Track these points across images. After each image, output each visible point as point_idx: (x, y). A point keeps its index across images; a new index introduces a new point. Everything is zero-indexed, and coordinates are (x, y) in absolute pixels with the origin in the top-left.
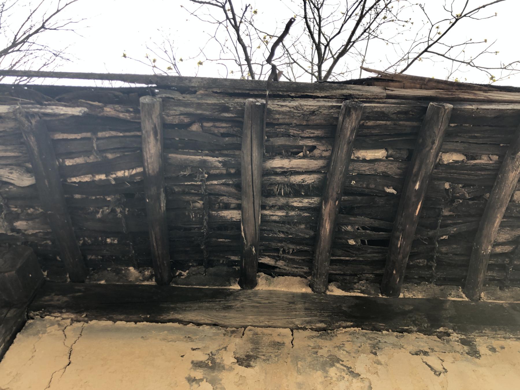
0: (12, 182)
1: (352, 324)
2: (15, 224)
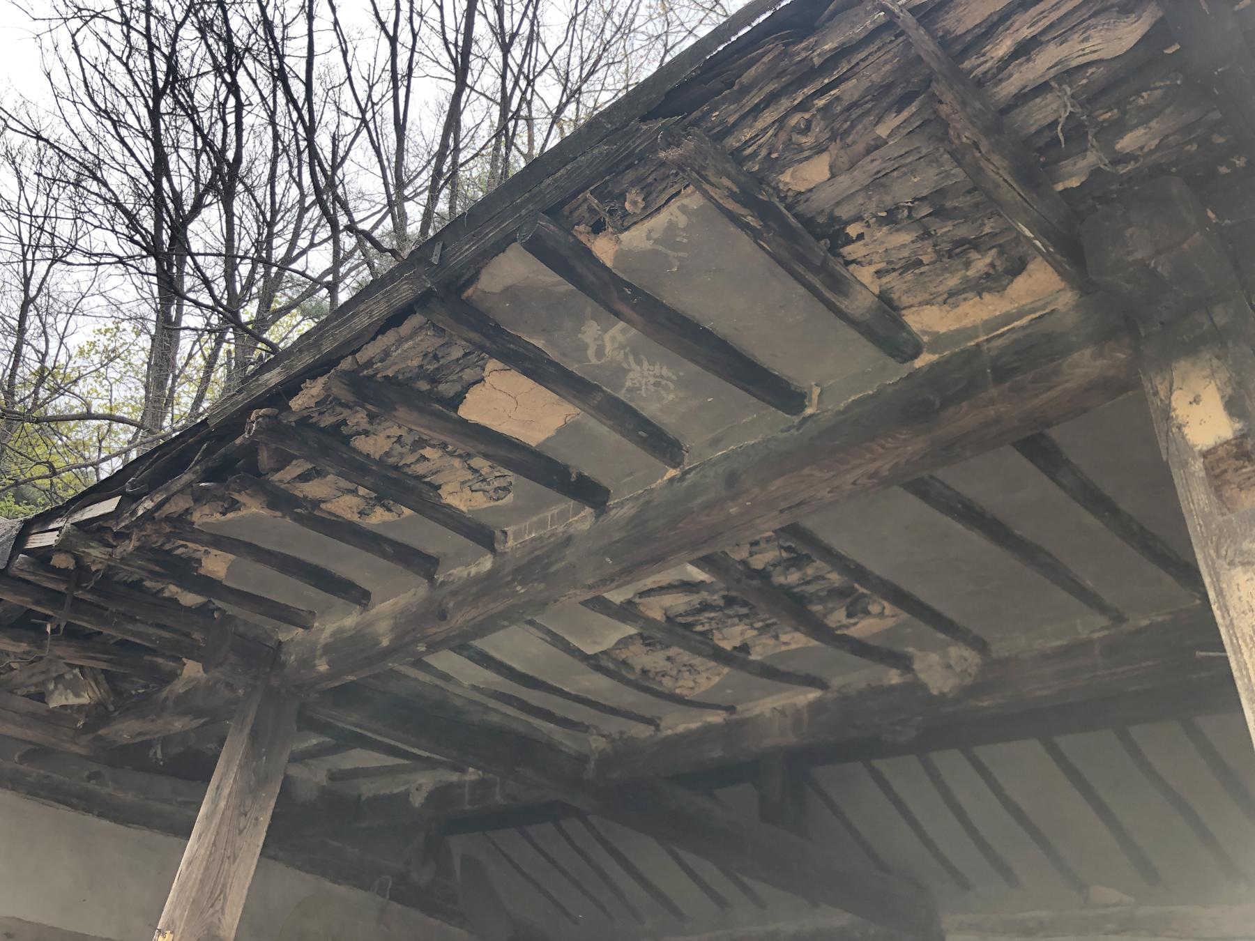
0: (1095, 57)
1: (452, 135)
2: (1118, 147)
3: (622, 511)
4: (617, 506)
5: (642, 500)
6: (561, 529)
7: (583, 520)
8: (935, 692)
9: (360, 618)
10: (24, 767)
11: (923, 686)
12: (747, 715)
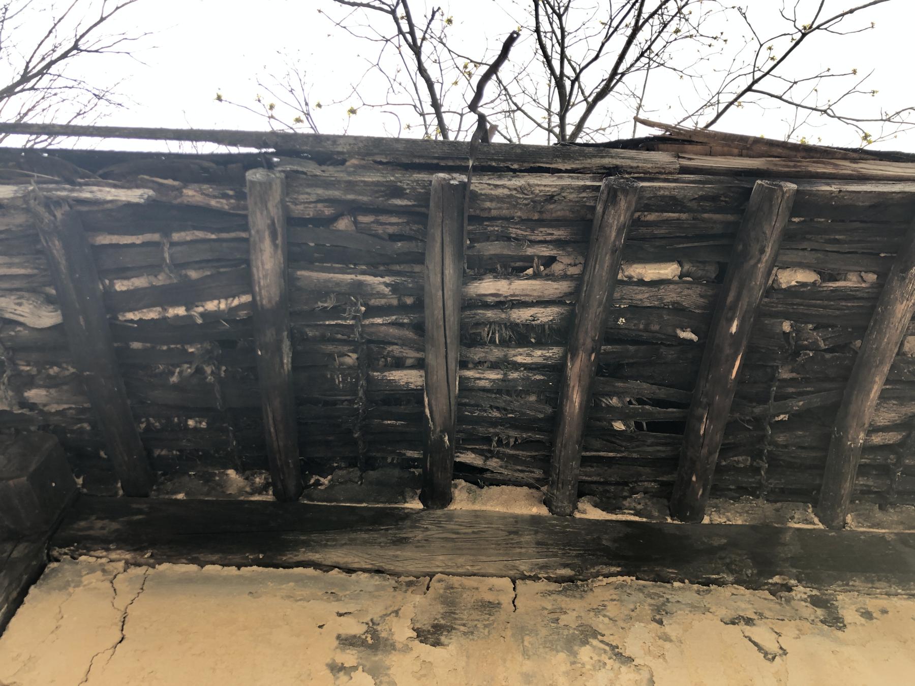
0: (21, 319)
1: (619, 569)
2: (26, 394)
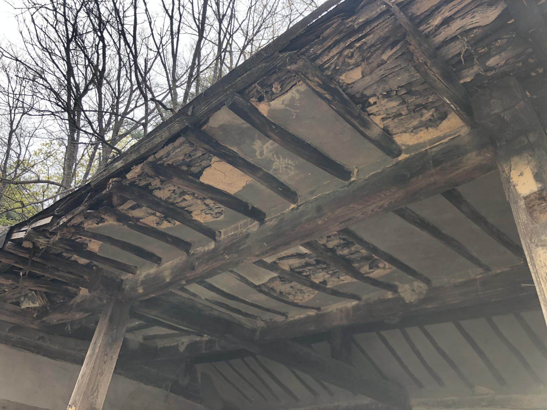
0: (477, 25)
1: (197, 59)
2: (487, 64)
3: (271, 223)
4: (269, 220)
5: (280, 218)
6: (244, 231)
7: (254, 226)
8: (408, 302)
9: (157, 269)
10: (10, 334)
11: (402, 299)
12: (326, 311)
